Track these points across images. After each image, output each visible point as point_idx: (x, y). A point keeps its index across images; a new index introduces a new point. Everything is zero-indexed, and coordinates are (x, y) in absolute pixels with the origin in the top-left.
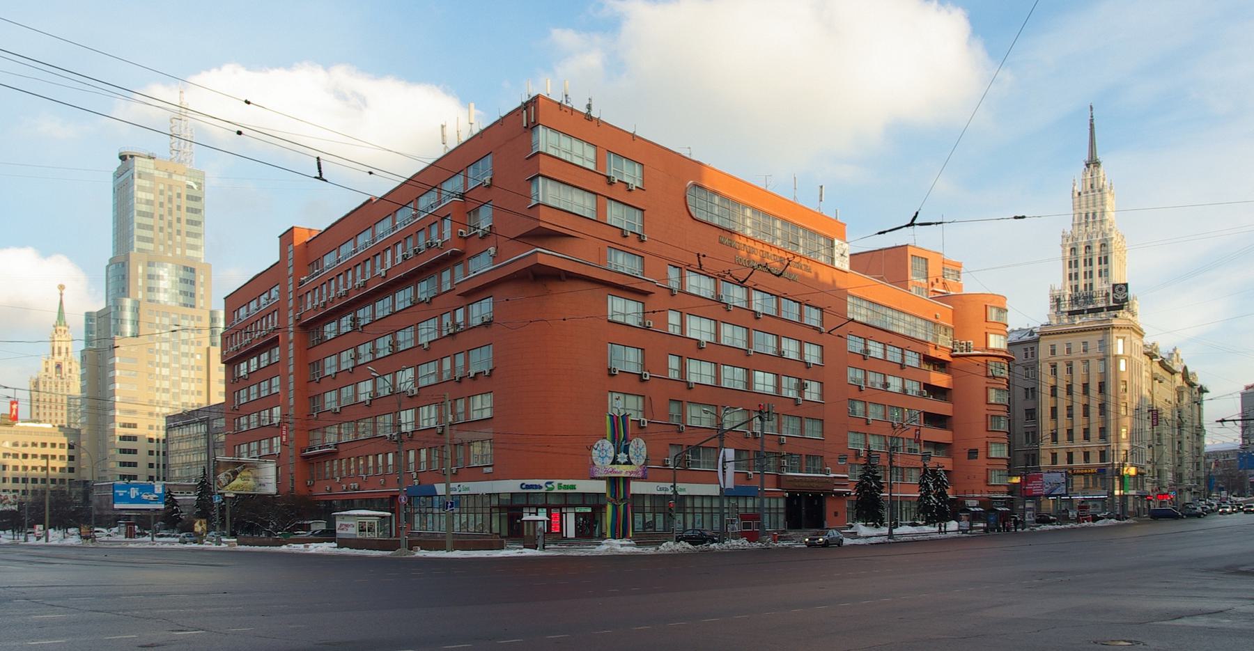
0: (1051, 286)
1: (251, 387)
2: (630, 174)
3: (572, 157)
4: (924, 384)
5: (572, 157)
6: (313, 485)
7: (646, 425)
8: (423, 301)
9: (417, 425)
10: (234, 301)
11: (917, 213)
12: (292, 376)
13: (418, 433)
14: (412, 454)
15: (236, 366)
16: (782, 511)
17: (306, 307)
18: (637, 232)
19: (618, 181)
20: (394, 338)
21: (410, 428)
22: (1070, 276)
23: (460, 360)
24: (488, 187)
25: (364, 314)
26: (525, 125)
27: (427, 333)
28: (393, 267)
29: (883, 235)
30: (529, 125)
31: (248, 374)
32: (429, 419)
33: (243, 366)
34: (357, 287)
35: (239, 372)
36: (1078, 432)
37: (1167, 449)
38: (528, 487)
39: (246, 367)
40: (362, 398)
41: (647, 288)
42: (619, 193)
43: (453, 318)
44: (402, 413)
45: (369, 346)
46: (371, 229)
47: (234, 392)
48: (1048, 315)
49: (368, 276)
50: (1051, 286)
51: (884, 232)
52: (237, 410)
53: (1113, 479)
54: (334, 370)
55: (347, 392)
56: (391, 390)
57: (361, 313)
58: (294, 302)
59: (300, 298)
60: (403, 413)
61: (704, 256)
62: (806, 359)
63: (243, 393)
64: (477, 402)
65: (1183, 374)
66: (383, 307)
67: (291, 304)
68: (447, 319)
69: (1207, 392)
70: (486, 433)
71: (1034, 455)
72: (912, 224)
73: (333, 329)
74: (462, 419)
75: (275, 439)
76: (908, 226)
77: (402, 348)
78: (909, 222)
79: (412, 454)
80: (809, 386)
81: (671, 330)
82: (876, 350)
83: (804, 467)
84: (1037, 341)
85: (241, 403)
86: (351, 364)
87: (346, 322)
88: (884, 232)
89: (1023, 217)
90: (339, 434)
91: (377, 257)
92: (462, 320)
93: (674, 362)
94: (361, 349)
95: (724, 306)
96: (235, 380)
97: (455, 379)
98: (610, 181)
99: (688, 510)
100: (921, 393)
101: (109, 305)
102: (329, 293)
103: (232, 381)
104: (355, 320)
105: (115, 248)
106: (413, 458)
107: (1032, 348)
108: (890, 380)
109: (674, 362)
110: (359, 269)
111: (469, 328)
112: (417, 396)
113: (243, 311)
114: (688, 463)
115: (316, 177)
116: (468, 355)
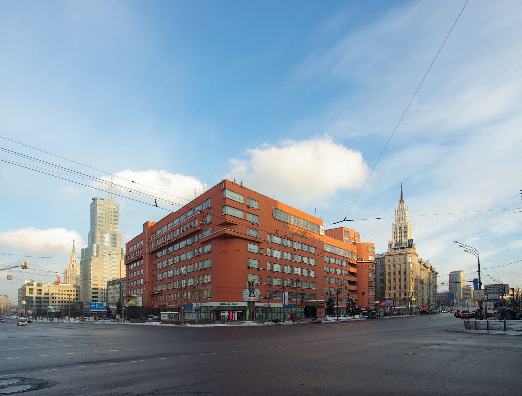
2: (255, 205)
4: (348, 271)
9: (187, 285)
11: (346, 217)
14: (185, 294)
17: (151, 247)
18: (257, 223)
19: (251, 207)
20: (180, 257)
21: (185, 285)
23: (201, 264)
26: (221, 189)
27: (190, 255)
28: (179, 234)
32: (191, 282)
33: (132, 266)
35: (130, 267)
37: (425, 292)
38: (222, 304)
40: (169, 276)
41: (260, 241)
42: (251, 211)
45: (171, 259)
49: (171, 237)
51: (335, 223)
53: (408, 302)
54: (160, 267)
55: (165, 274)
57: (169, 249)
59: (150, 244)
60: (182, 281)
61: (278, 231)
63: (132, 274)
64: (206, 277)
66: (176, 247)
67: (147, 246)
69: (438, 274)
70: (209, 287)
72: (344, 221)
74: (201, 282)
75: (142, 289)
76: (343, 221)
78: (343, 220)
79: (185, 294)
80: (311, 272)
81: (268, 254)
82: (333, 261)
83: (310, 298)
84: (384, 258)
86: (166, 265)
87: (164, 252)
88: (335, 223)
89: (380, 218)
90: (162, 287)
93: (268, 265)
94: (169, 260)
98: (248, 207)
100: (347, 274)
102: (159, 242)
104: (167, 251)
107: (383, 260)
108: (337, 270)
109: (268, 265)
112: (187, 275)
113: (131, 248)
115: (155, 206)
116: (203, 262)
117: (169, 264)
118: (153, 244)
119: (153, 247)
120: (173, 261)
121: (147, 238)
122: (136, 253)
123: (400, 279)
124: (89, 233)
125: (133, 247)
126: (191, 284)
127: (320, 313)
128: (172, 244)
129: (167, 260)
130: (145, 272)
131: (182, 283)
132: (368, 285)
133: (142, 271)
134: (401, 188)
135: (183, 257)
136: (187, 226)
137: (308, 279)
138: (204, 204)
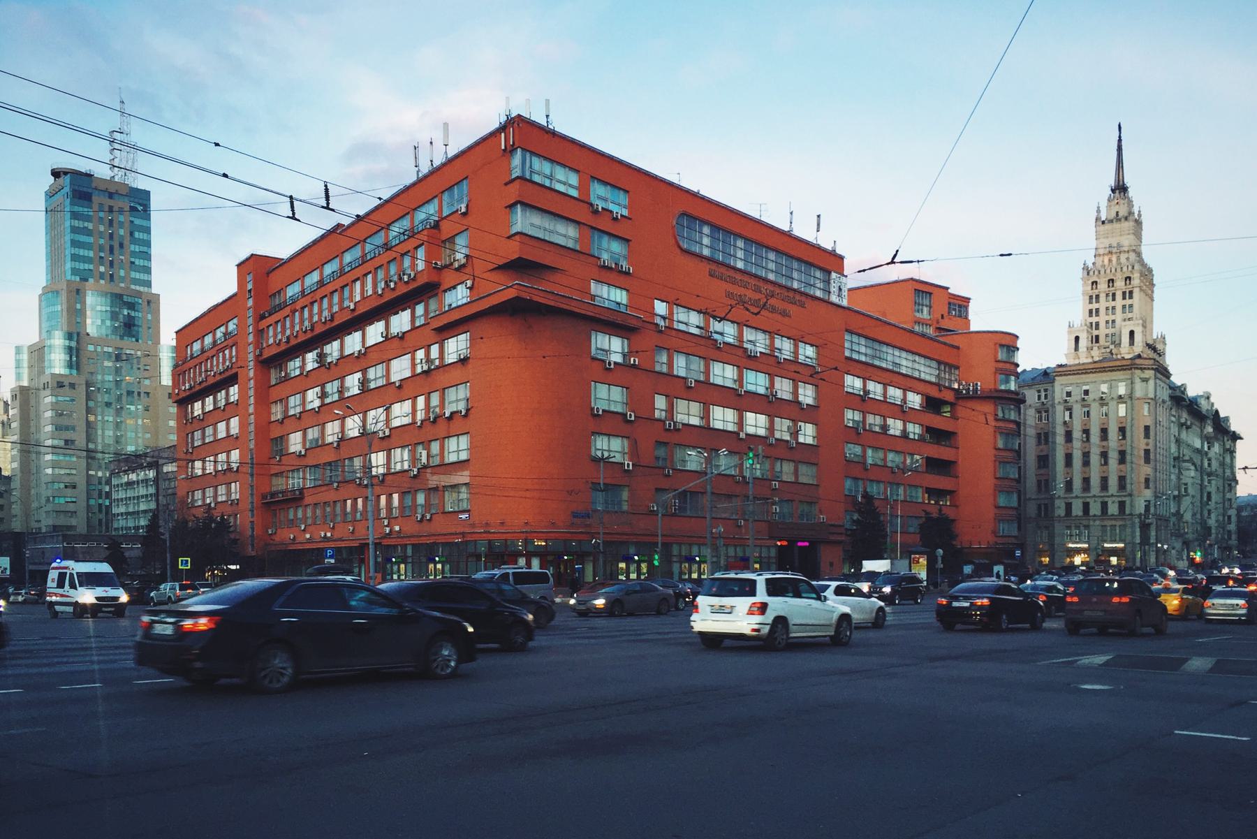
0: (1070, 323)
1: (195, 433)
3: (551, 183)
5: (551, 183)
6: (275, 533)
7: (612, 366)
8: (395, 336)
9: (389, 468)
10: (185, 334)
11: (897, 251)
12: (252, 416)
13: (390, 476)
14: (383, 499)
15: (190, 406)
16: (774, 561)
17: (267, 342)
20: (364, 374)
21: (381, 470)
22: (1091, 311)
23: (435, 399)
24: (464, 214)
25: (333, 349)
26: (503, 148)
27: (400, 369)
28: (363, 298)
29: (862, 273)
30: (508, 147)
31: (204, 414)
32: (402, 461)
34: (323, 320)
35: (192, 413)
36: (1095, 482)
39: (200, 407)
40: (329, 439)
41: (633, 323)
42: (605, 224)
43: (428, 354)
44: (372, 455)
45: (336, 384)
46: (338, 258)
47: (188, 434)
48: (1065, 355)
49: (336, 309)
50: (1070, 323)
51: (864, 271)
52: (192, 453)
54: (298, 410)
55: (313, 433)
56: (361, 431)
57: (327, 349)
58: (254, 336)
59: (260, 333)
60: (373, 456)
62: (800, 399)
63: (198, 435)
64: (452, 444)
65: (1213, 419)
66: (353, 343)
67: (251, 338)
68: (420, 354)
69: (1241, 438)
70: (463, 477)
71: (1046, 505)
72: (893, 262)
73: (379, 374)
74: (437, 461)
75: (233, 484)
76: (888, 264)
77: (372, 385)
78: (890, 261)
79: (383, 499)
80: (803, 428)
81: (658, 368)
85: (195, 445)
86: (317, 403)
87: (311, 358)
88: (864, 271)
89: (1010, 255)
90: (304, 478)
91: (345, 289)
92: (437, 356)
94: (329, 388)
95: (713, 342)
96: (187, 420)
97: (430, 419)
99: (675, 559)
101: (42, 338)
102: (293, 326)
103: (185, 422)
104: (321, 357)
105: (49, 275)
106: (385, 503)
107: (1046, 390)
108: (890, 421)
110: (325, 301)
111: (443, 366)
112: (388, 436)
113: (197, 346)
114: (675, 509)
115: (288, 217)
116: (444, 394)
117: (328, 400)
118: (271, 333)
119: (271, 341)
120: (323, 395)
121: (250, 313)
122: (206, 366)
123: (1086, 455)
124: (43, 294)
125: (203, 342)
126: (402, 466)
127: (831, 564)
128: (339, 331)
129: (323, 386)
130: (242, 425)
131: (374, 464)
132: (995, 475)
133: (234, 422)
134: (1120, 140)
135: (375, 375)
136: (388, 271)
137: (793, 451)
138: (446, 196)
